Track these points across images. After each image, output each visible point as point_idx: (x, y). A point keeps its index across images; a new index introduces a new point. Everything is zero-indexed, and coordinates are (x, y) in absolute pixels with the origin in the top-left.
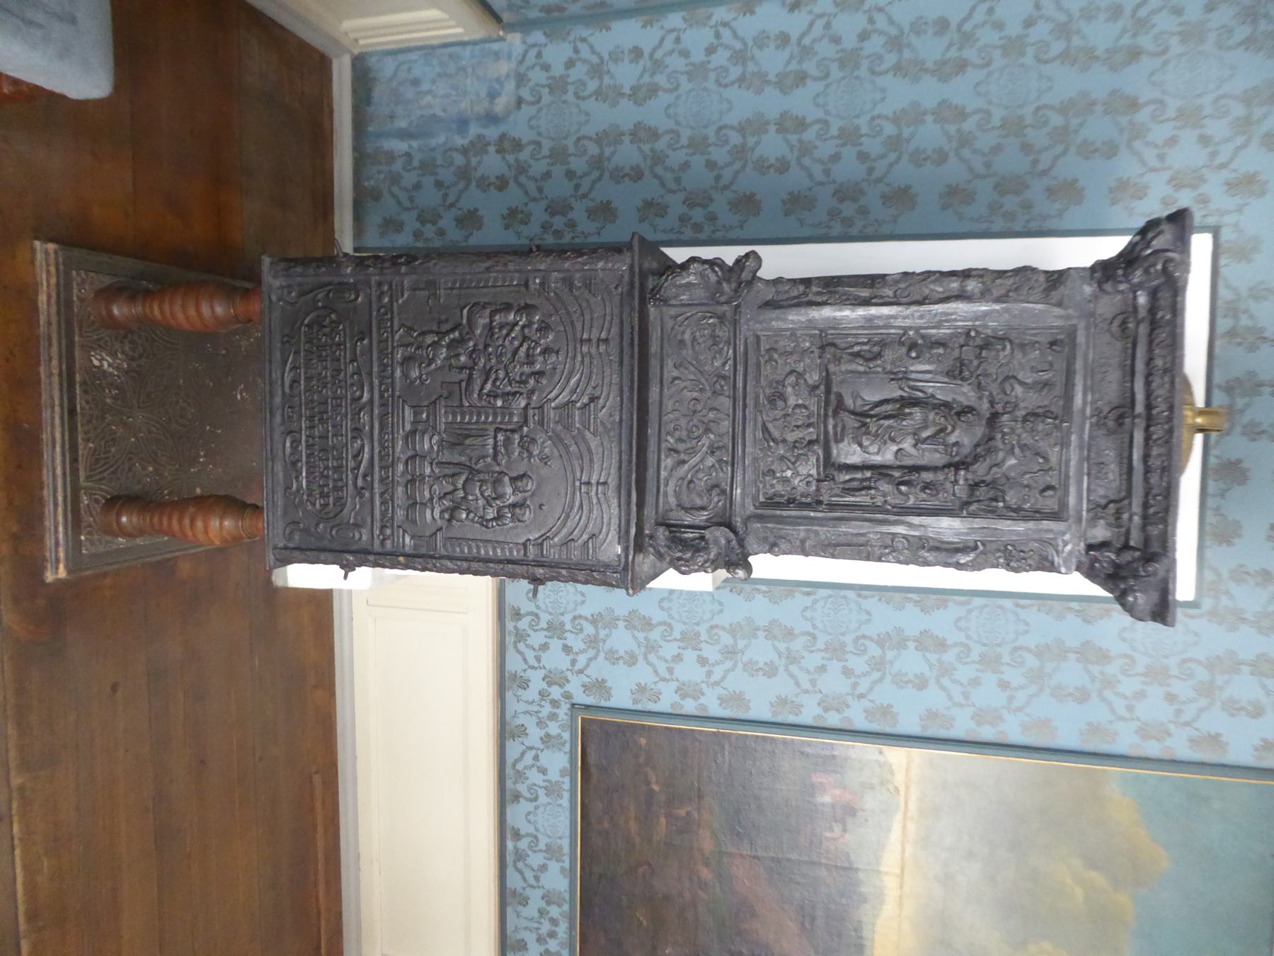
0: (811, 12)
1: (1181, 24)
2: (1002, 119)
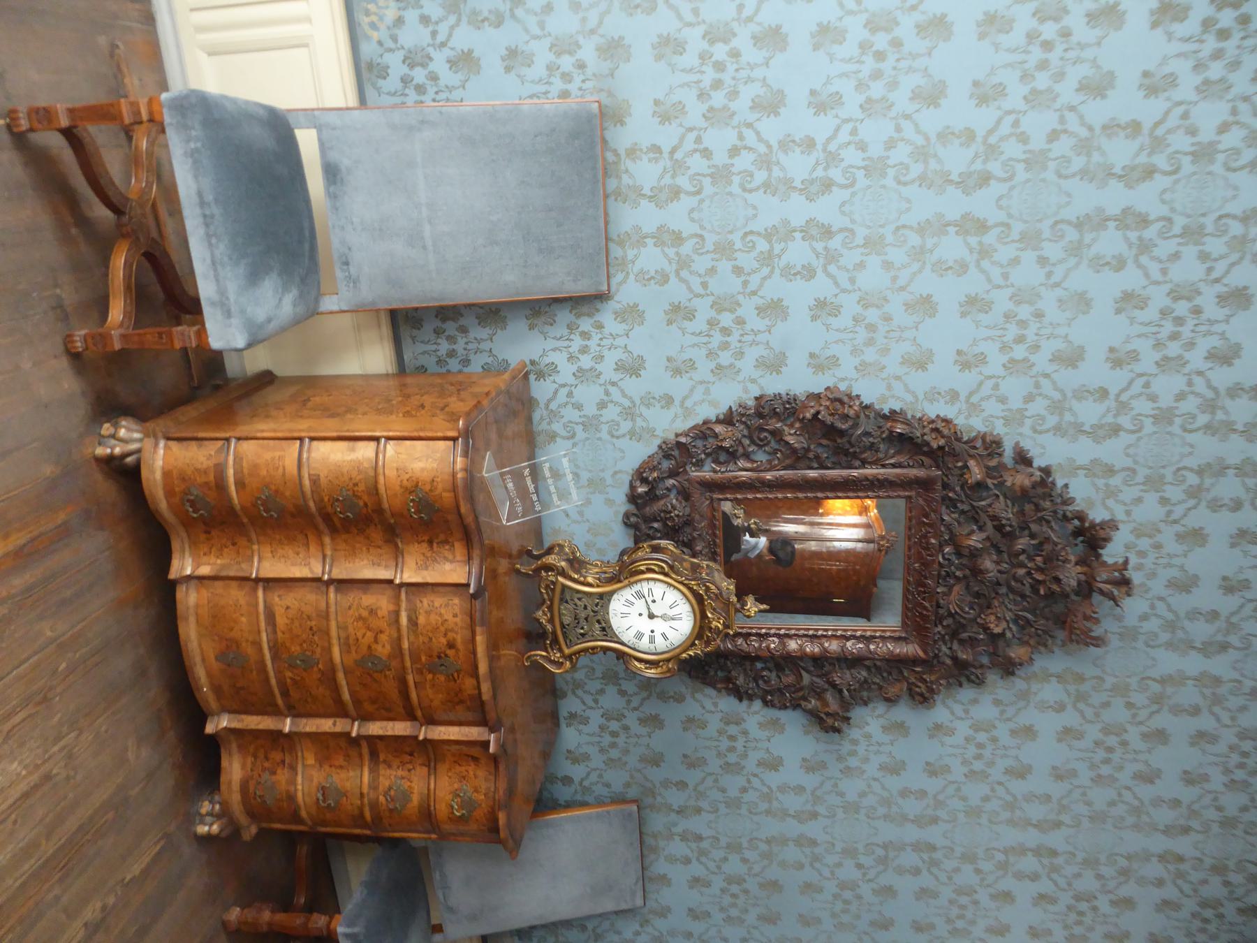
0: (681, 125)
1: (1193, 144)
2: (1183, 228)
